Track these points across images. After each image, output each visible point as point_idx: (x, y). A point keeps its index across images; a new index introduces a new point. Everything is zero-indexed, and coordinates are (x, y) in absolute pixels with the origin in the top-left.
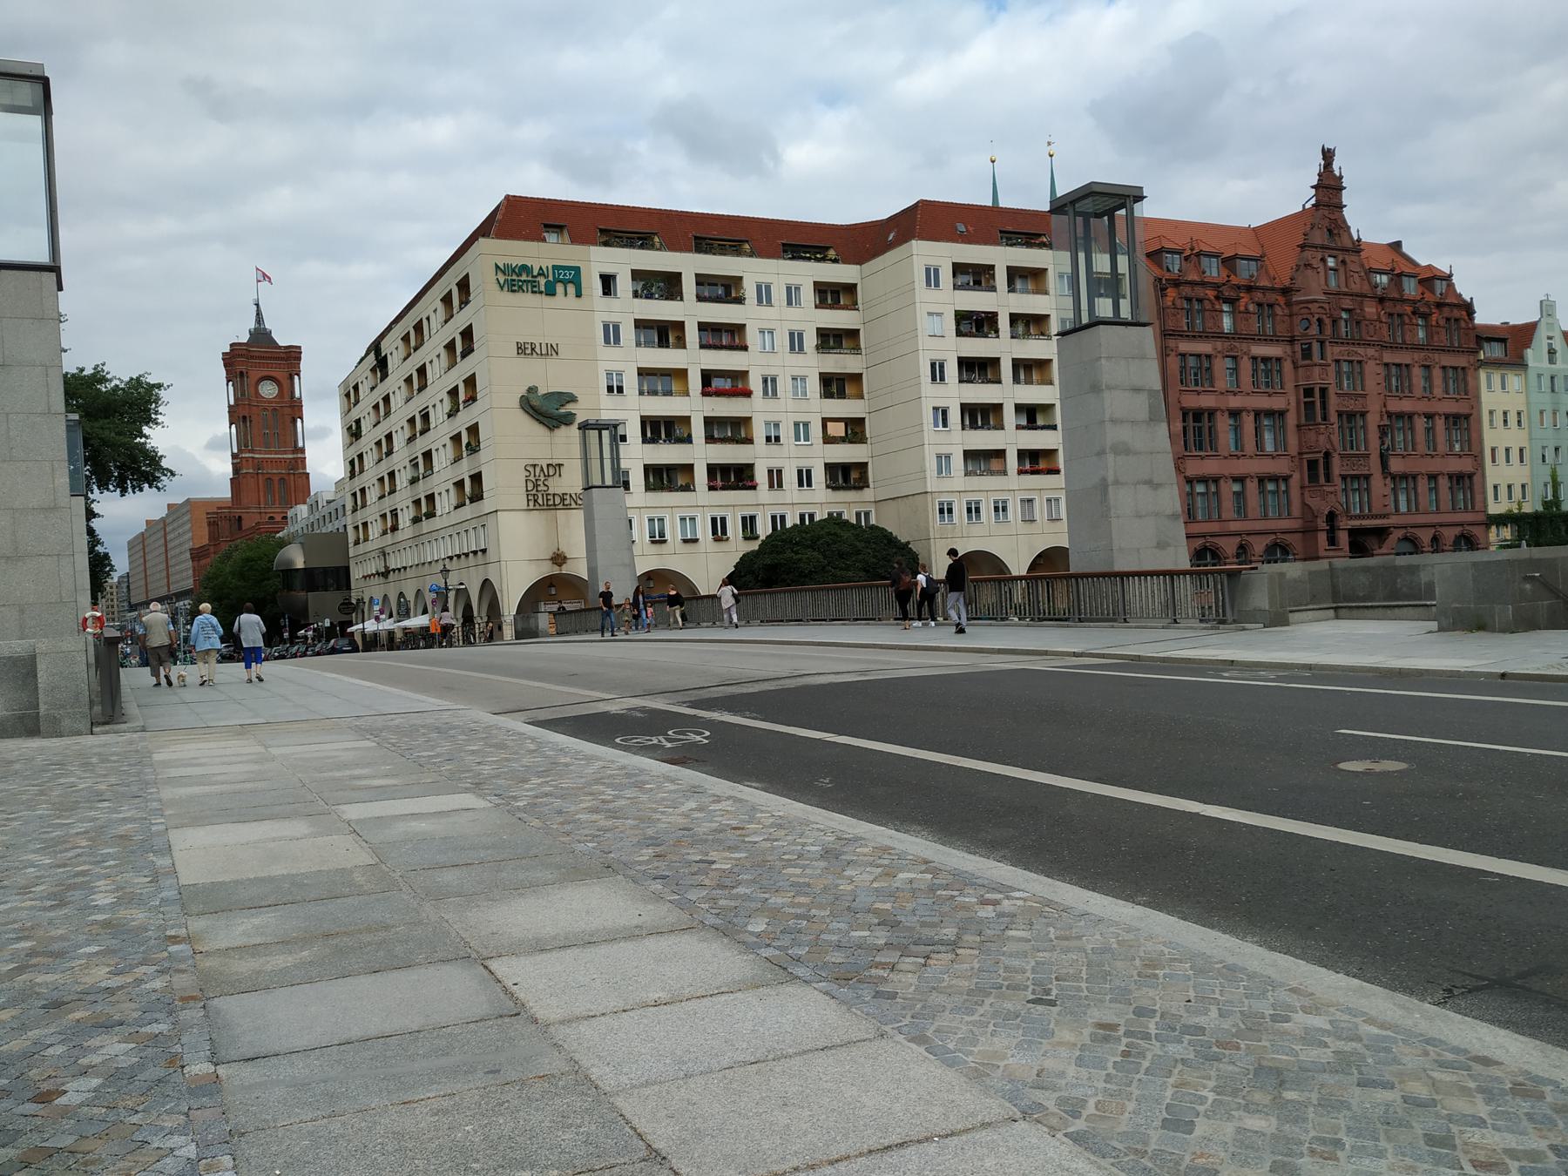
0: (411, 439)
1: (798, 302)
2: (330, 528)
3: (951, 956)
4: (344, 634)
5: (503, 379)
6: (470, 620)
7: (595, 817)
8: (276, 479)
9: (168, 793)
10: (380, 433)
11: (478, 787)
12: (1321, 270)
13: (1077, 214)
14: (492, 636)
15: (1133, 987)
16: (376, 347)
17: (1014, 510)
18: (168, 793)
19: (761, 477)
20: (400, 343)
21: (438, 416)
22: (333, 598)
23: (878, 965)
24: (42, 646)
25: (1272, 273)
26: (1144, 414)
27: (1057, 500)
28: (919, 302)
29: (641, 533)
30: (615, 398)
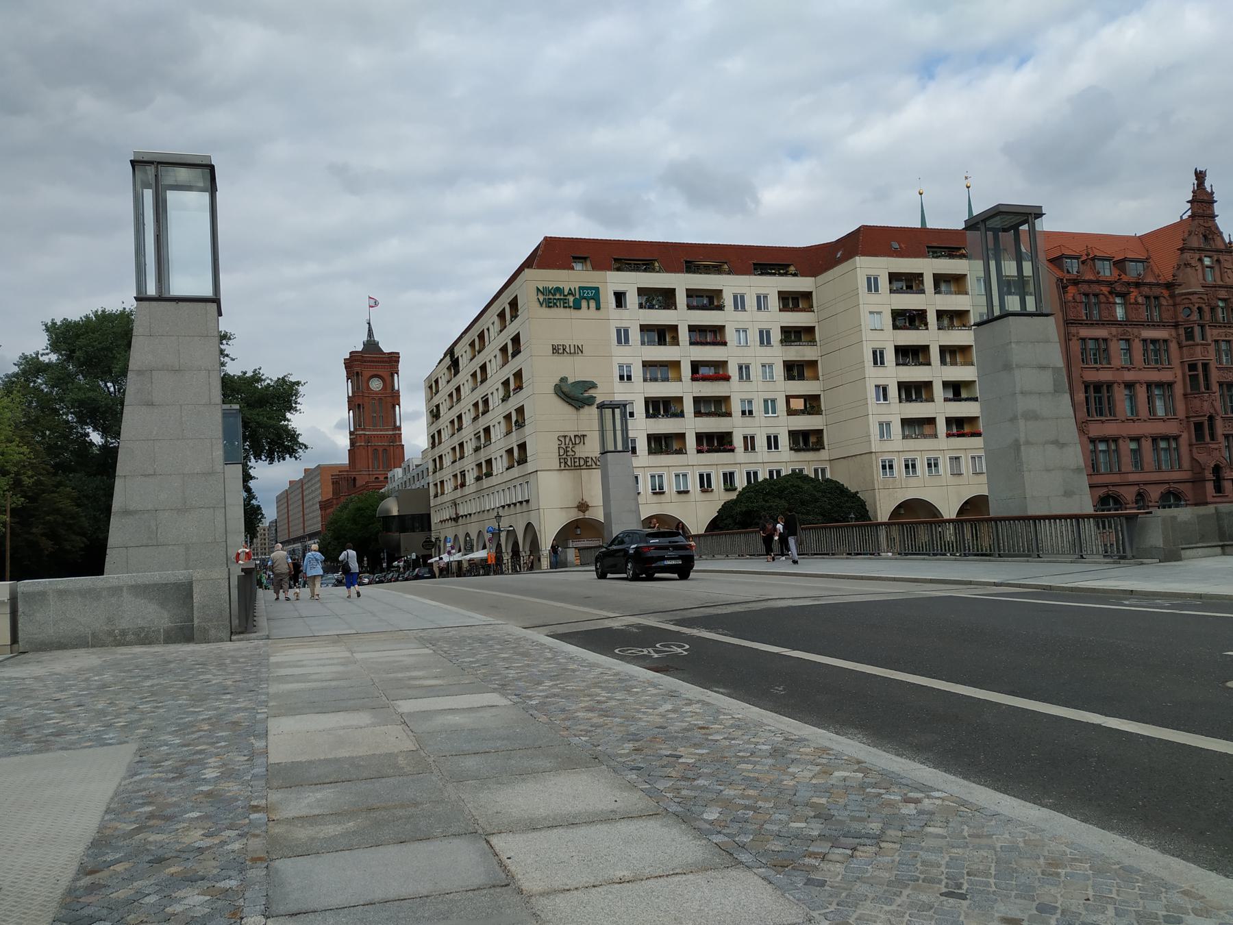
0: (475, 419)
1: (766, 307)
2: (418, 485)
3: (874, 849)
4: (425, 564)
5: (542, 372)
6: (513, 554)
7: (591, 715)
8: (381, 449)
9: (274, 688)
10: (453, 414)
11: (503, 689)
12: (1199, 268)
13: (987, 229)
14: (533, 566)
15: (1037, 884)
16: (450, 352)
17: (944, 466)
18: (274, 688)
19: (738, 442)
20: (468, 348)
21: (494, 401)
22: (419, 537)
23: (813, 855)
24: (197, 574)
25: (1157, 271)
26: (1049, 387)
27: (980, 457)
28: (864, 306)
29: (645, 486)
30: (626, 385)
